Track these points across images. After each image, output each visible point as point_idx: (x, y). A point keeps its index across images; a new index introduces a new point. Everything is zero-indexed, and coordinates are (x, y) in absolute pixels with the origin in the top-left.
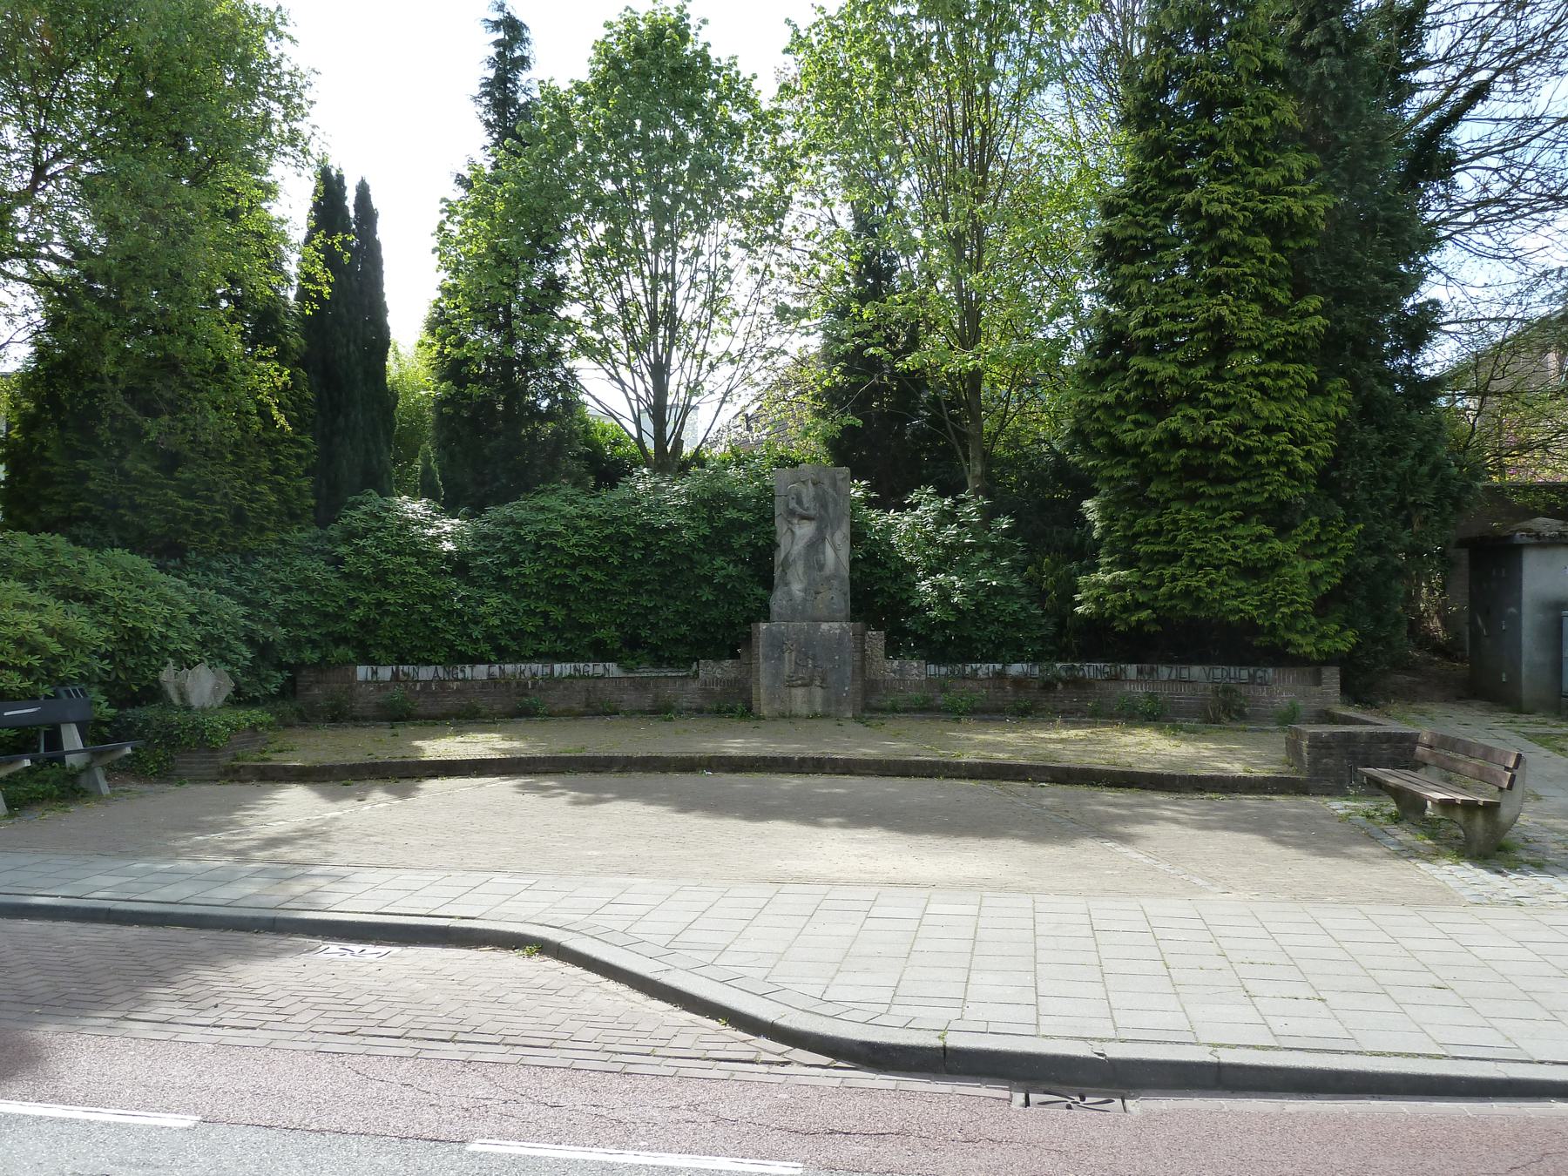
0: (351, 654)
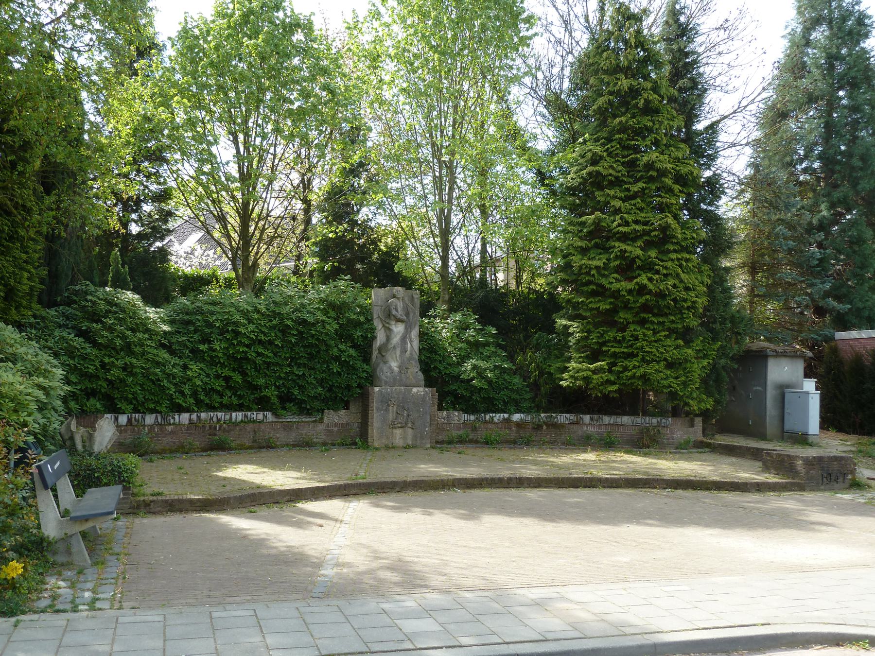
0: (98, 405)
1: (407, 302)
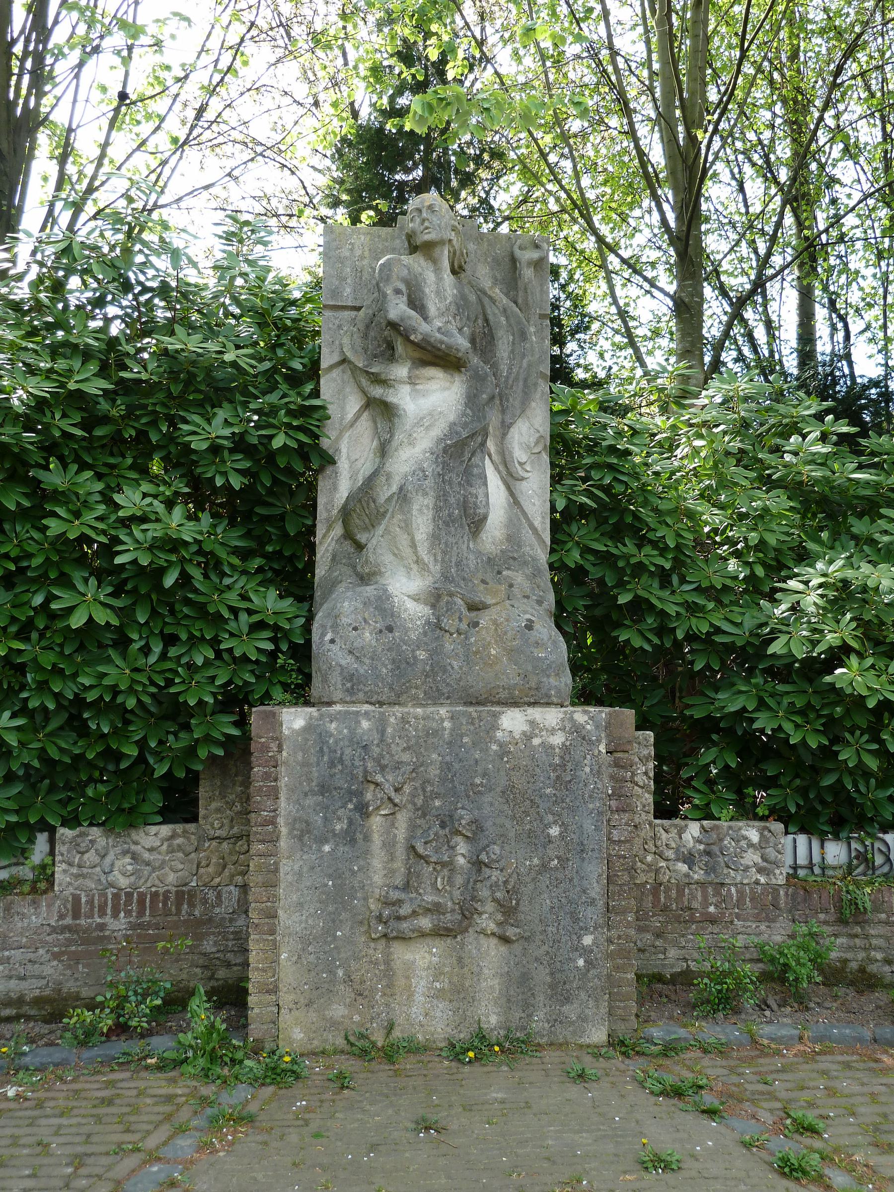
1: (486, 284)
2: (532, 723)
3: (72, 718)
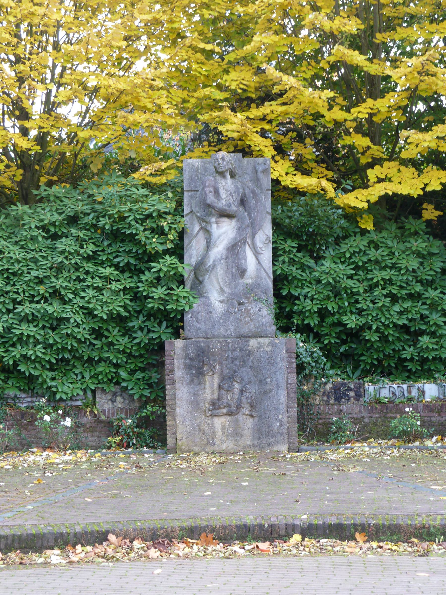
2: (259, 343)
3: (428, 285)
